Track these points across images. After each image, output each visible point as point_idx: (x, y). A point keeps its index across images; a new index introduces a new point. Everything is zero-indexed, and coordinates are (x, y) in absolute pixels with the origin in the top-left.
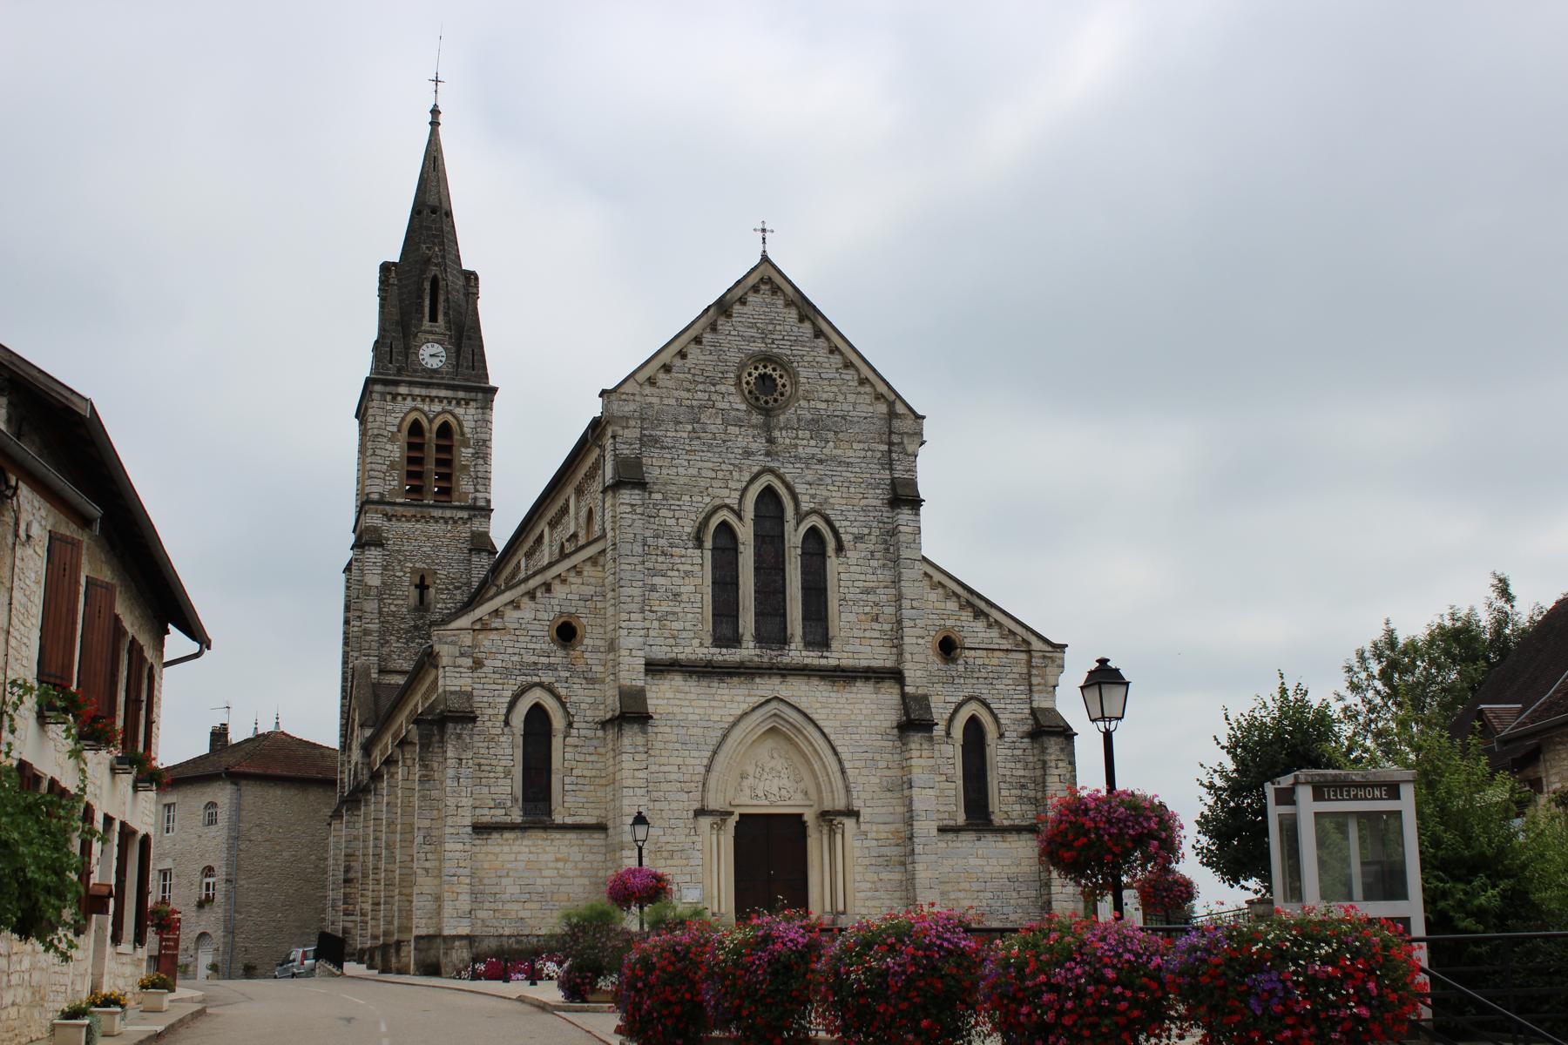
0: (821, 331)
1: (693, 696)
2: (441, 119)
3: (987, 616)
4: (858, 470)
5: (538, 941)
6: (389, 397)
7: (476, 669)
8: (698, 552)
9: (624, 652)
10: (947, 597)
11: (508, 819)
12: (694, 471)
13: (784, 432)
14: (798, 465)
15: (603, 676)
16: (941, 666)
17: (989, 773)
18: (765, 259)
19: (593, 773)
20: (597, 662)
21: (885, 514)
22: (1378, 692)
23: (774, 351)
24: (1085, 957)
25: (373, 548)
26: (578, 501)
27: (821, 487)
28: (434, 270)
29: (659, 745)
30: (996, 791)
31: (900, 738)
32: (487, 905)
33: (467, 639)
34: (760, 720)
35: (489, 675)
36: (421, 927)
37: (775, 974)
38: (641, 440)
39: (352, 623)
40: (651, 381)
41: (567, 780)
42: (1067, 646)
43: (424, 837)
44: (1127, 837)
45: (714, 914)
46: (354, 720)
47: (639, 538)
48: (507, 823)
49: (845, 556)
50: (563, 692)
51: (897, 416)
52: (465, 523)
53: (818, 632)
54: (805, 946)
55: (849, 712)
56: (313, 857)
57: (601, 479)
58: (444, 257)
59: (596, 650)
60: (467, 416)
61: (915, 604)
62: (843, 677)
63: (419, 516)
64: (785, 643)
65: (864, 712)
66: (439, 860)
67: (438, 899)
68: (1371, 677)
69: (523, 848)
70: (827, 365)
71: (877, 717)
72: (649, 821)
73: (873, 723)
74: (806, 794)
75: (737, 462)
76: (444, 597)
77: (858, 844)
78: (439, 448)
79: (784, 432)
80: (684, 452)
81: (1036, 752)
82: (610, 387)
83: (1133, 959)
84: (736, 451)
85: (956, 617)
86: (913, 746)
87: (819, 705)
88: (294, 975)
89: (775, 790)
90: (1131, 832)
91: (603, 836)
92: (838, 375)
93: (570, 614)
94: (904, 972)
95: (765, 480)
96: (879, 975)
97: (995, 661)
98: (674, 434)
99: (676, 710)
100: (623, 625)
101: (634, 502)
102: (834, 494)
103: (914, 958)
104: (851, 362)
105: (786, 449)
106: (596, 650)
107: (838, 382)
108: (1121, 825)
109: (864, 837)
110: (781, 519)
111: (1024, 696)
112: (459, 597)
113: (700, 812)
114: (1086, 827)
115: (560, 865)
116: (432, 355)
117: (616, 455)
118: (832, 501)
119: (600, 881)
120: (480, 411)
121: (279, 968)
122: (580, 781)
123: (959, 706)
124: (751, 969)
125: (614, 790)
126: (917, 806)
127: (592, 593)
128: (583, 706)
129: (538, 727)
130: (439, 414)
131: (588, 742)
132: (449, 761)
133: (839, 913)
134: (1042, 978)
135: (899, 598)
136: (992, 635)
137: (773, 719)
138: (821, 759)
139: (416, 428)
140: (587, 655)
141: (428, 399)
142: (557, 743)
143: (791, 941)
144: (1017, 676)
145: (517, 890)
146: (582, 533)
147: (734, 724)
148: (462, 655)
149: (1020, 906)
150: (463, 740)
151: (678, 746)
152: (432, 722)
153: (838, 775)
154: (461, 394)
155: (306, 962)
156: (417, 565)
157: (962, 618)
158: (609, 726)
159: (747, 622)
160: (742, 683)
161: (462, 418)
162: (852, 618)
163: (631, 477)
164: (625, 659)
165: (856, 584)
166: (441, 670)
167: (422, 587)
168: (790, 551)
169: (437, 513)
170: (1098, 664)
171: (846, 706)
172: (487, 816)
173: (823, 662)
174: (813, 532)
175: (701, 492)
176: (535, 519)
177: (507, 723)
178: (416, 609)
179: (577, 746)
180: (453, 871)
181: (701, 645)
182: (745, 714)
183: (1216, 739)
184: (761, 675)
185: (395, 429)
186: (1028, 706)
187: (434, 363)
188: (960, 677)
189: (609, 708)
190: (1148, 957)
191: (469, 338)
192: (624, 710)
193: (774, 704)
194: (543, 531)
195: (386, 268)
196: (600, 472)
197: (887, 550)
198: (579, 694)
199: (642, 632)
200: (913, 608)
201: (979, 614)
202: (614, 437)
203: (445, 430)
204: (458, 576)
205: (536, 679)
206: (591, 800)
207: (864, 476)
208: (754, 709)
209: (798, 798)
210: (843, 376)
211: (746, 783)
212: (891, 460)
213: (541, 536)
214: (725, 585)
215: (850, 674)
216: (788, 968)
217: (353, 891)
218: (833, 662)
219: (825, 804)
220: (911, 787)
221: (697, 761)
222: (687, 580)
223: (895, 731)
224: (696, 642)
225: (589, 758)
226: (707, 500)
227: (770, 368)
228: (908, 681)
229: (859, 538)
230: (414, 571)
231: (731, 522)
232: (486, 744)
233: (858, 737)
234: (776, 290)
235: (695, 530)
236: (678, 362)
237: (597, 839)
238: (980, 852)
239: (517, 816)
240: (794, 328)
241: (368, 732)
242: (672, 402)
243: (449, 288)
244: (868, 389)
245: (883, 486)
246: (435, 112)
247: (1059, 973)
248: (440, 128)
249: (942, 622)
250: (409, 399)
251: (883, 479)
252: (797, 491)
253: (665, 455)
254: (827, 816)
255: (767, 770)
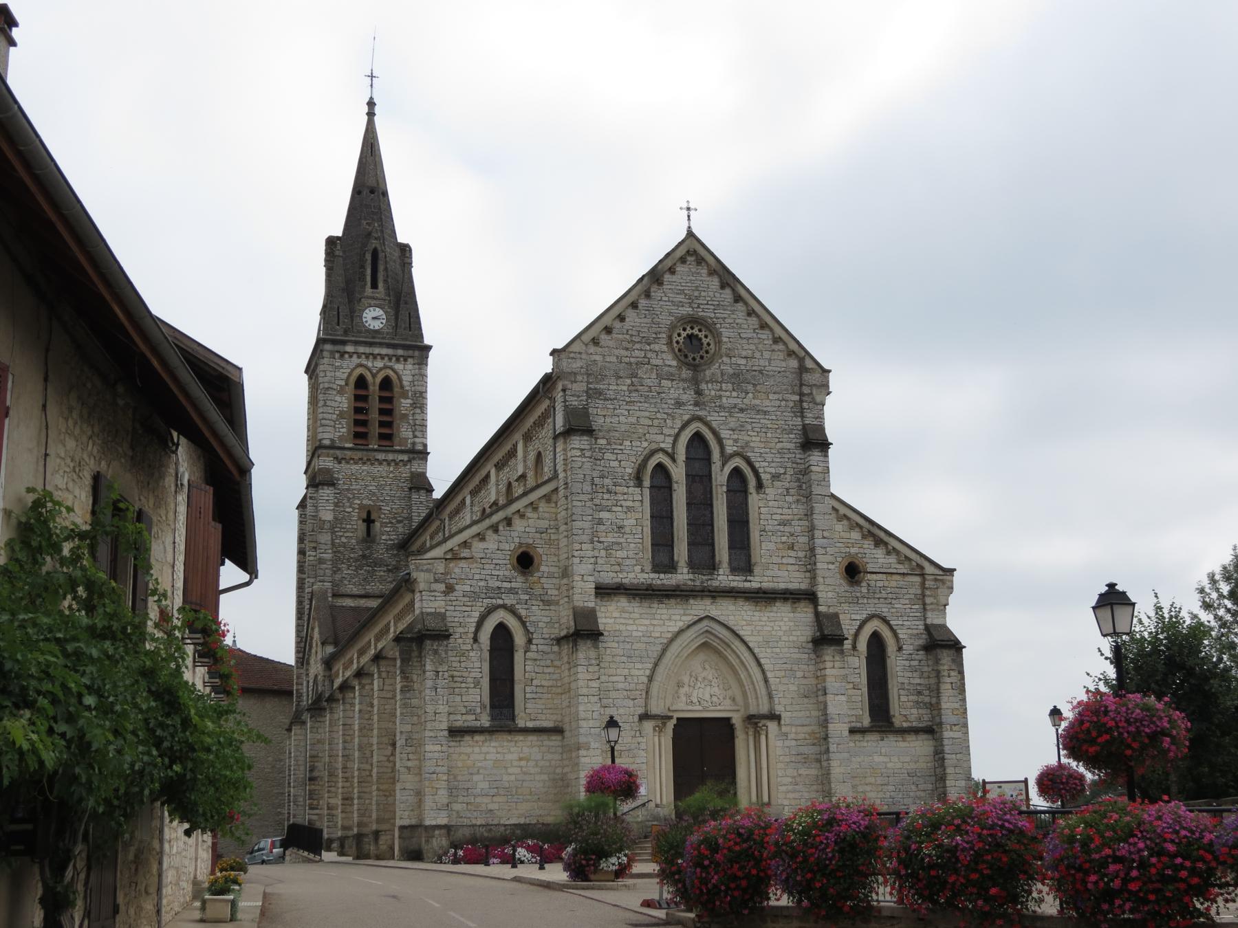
0: (740, 296)
1: (637, 616)
2: (377, 110)
3: (886, 544)
4: (774, 417)
5: (505, 830)
6: (337, 355)
7: (448, 593)
8: (638, 490)
9: (577, 578)
10: (851, 528)
11: (478, 724)
12: (634, 420)
13: (710, 385)
14: (722, 414)
15: (557, 598)
16: (847, 588)
17: (889, 681)
18: (690, 234)
19: (550, 683)
20: (552, 586)
21: (798, 456)
22: (1228, 611)
23: (700, 314)
24: (1145, 834)
25: (326, 487)
26: (525, 446)
27: (742, 433)
28: (374, 243)
29: (608, 658)
30: (896, 697)
31: (815, 651)
32: (461, 799)
33: (440, 567)
34: (694, 636)
35: (460, 599)
36: (403, 817)
37: (842, 851)
38: (587, 392)
39: (308, 553)
40: (595, 342)
41: (528, 689)
42: (955, 570)
43: (406, 740)
44: (1143, 734)
45: (657, 806)
46: (312, 638)
47: (588, 478)
48: (477, 727)
49: (764, 493)
50: (523, 613)
51: (807, 370)
52: (405, 465)
53: (743, 562)
54: (866, 828)
55: (769, 629)
56: (270, 759)
57: (551, 427)
58: (382, 232)
59: (551, 576)
60: (405, 370)
61: (826, 534)
62: (765, 598)
63: (365, 459)
64: (714, 569)
65: (784, 628)
66: (420, 760)
67: (419, 794)
68: (1221, 596)
69: (491, 749)
70: (746, 326)
71: (794, 633)
72: (620, 724)
73: (791, 638)
74: (734, 700)
75: (670, 411)
76: (388, 529)
77: (780, 743)
78: (382, 399)
79: (710, 385)
80: (624, 403)
81: (930, 663)
82: (560, 346)
83: (1189, 835)
84: (669, 401)
85: (859, 545)
86: (827, 658)
87: (744, 623)
88: (263, 862)
89: (707, 697)
90: (1147, 730)
91: (559, 738)
92: (755, 335)
93: (528, 545)
94: (972, 848)
95: (695, 427)
96: (948, 851)
97: (894, 584)
98: (615, 387)
99: (622, 628)
100: (576, 554)
101: (583, 447)
102: (754, 439)
103: (980, 835)
104: (766, 323)
105: (712, 400)
106: (551, 576)
107: (756, 341)
108: (1138, 724)
109: (785, 737)
110: (708, 460)
111: (919, 614)
112: (401, 530)
113: (645, 717)
114: (1108, 726)
115: (523, 763)
116: (374, 318)
117: (566, 406)
118: (752, 444)
119: (557, 777)
120: (417, 366)
121: (249, 856)
122: (539, 690)
123: (863, 623)
124: (820, 848)
125: (570, 698)
126: (831, 710)
127: (547, 526)
128: (540, 624)
129: (502, 642)
130: (381, 369)
131: (545, 657)
132: (428, 673)
133: (763, 805)
134: (1108, 851)
135: (812, 529)
136: (890, 561)
137: (705, 635)
138: (747, 670)
139: (361, 382)
140: (543, 580)
141: (371, 357)
142: (518, 657)
143: (854, 823)
144: (913, 596)
145: (485, 785)
146: (530, 474)
147: (672, 640)
148: (436, 581)
149: (919, 798)
150: (440, 655)
151: (624, 659)
152: (411, 640)
153: (762, 683)
154: (400, 352)
155: (274, 850)
156: (364, 502)
157: (865, 546)
158: (563, 642)
159: (681, 550)
160: (678, 603)
161: (401, 373)
162: (772, 546)
163: (580, 426)
164: (579, 584)
165: (774, 517)
166: (417, 595)
167: (369, 521)
168: (717, 488)
169: (381, 456)
170: (1107, 588)
171: (768, 623)
172: (460, 721)
173: (747, 585)
174: (737, 472)
175: (640, 438)
176: (482, 461)
177: (475, 640)
178: (364, 541)
179: (535, 660)
180: (433, 769)
181: (642, 571)
182: (681, 631)
183: (1100, 651)
184: (695, 597)
185: (343, 383)
186: (922, 623)
187: (376, 325)
188: (863, 597)
189: (563, 627)
190: (1200, 833)
191: (406, 303)
192: (579, 628)
193: (705, 623)
194: (489, 472)
195: (331, 242)
196: (550, 420)
197: (801, 486)
198: (538, 615)
199: (592, 560)
200: (824, 538)
201: (879, 542)
202: (564, 390)
203: (386, 384)
204: (400, 511)
205: (500, 602)
206: (549, 706)
207: (779, 423)
208: (689, 627)
209: (727, 704)
210: (759, 336)
211: (683, 691)
212: (802, 408)
213: (488, 476)
214: (662, 518)
215: (664, 593)
216: (853, 846)
217: (317, 788)
218: (755, 585)
219: (751, 709)
220: (826, 694)
221: (641, 672)
222: (629, 515)
223: (810, 645)
224: (638, 568)
225: (547, 670)
226: (645, 444)
227: (696, 329)
228: (821, 601)
229: (775, 477)
230: (361, 507)
231: (666, 463)
232: (458, 659)
233: (778, 650)
234: (700, 261)
235: (635, 471)
236: (618, 325)
237: (555, 740)
238: (883, 751)
239: (485, 721)
240: (716, 294)
241: (330, 649)
242: (614, 359)
243: (388, 259)
244: (781, 347)
245: (796, 432)
246: (371, 104)
247: (1123, 848)
248: (376, 118)
249: (848, 550)
250: (355, 356)
251: (796, 426)
252: (722, 436)
253: (609, 406)
254: (754, 721)
255: (700, 679)
